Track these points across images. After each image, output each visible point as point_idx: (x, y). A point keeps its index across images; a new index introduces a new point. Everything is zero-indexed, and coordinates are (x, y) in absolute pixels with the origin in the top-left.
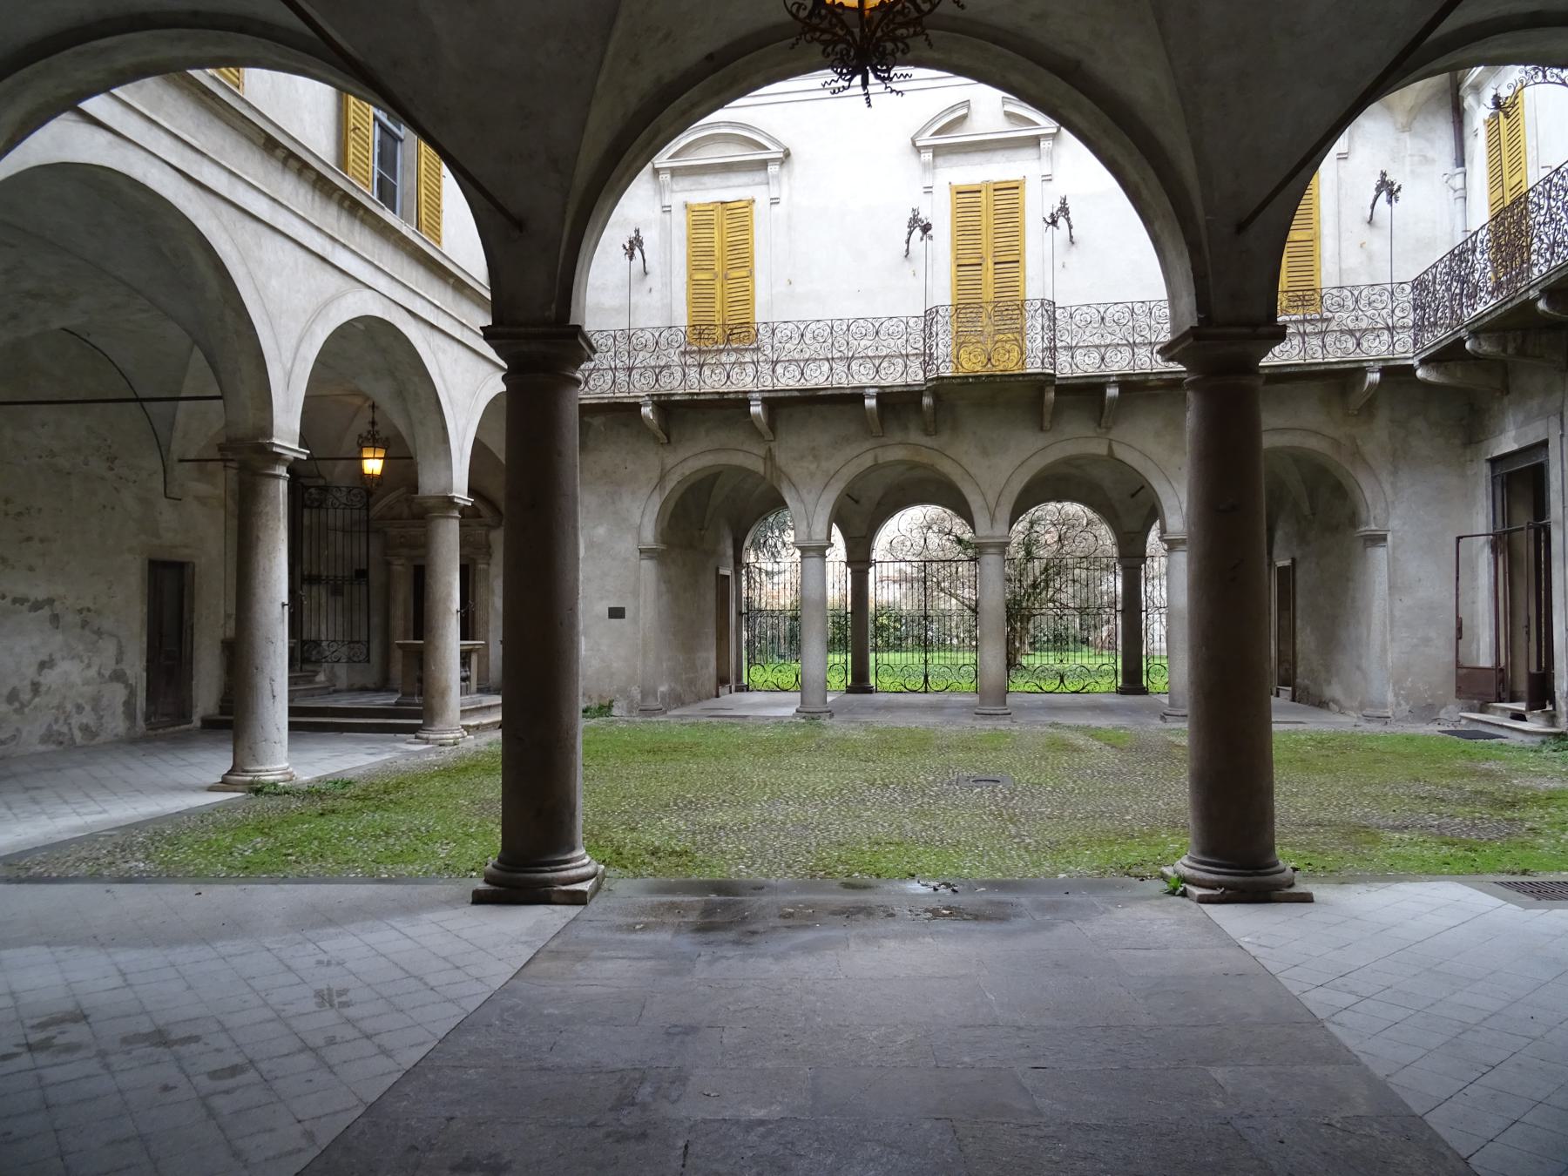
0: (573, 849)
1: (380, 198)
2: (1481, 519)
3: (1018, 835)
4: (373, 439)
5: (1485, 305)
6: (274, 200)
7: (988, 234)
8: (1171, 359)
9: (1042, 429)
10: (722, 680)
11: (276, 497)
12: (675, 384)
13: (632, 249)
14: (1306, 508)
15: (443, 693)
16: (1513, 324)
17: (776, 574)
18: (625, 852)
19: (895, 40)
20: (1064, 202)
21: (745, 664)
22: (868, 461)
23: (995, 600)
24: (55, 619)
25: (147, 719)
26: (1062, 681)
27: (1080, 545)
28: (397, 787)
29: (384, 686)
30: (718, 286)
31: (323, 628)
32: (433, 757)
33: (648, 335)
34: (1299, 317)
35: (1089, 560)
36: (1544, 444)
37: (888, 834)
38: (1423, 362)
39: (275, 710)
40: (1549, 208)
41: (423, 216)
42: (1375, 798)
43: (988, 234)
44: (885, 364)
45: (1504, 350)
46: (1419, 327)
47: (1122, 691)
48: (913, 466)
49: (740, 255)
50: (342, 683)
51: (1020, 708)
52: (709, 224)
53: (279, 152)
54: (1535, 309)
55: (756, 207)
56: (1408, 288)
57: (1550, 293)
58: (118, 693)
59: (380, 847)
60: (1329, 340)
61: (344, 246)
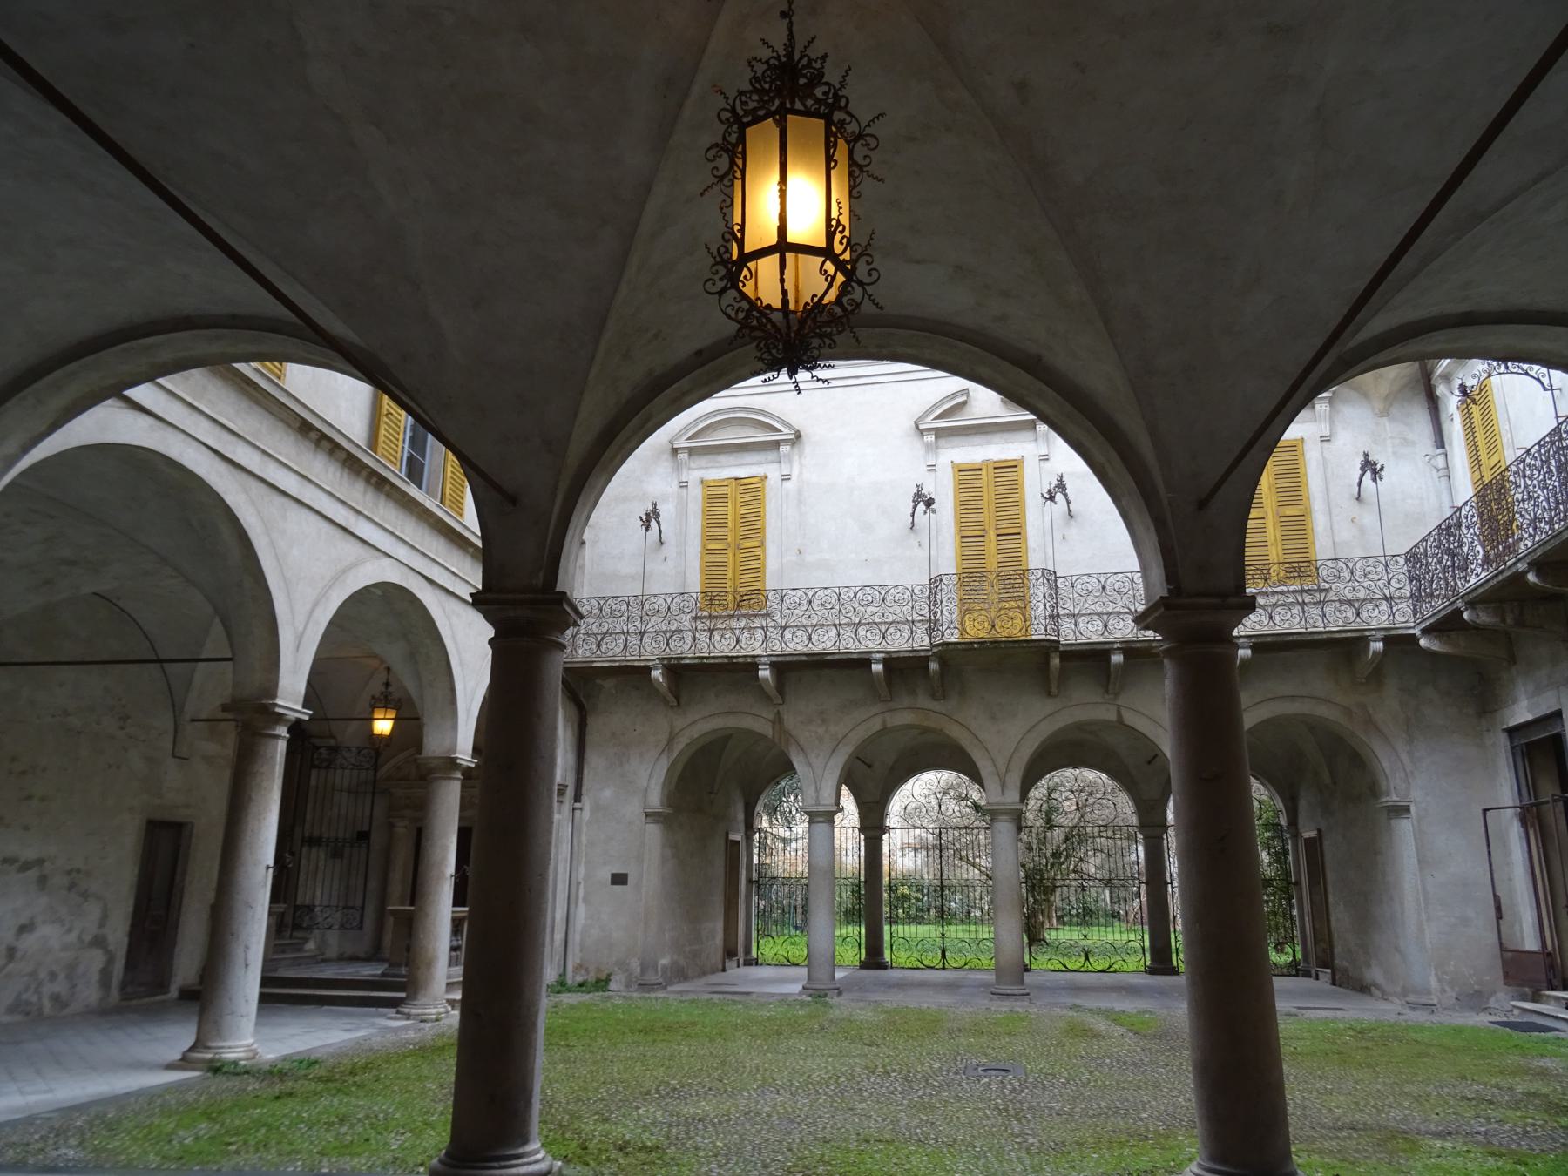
0: (526, 1141)
1: (409, 476)
2: (1505, 790)
3: (1022, 1134)
4: (385, 700)
5: (1477, 576)
6: (303, 477)
7: (990, 504)
8: (1146, 628)
9: (1049, 694)
10: (730, 953)
11: (273, 758)
12: (684, 648)
13: (648, 521)
14: (1326, 777)
15: (430, 965)
16: (1505, 594)
17: (784, 843)
18: (591, 1146)
19: (821, 336)
20: (1060, 479)
21: (754, 935)
22: (876, 725)
23: (1010, 875)
24: (42, 881)
25: (123, 987)
26: (1087, 958)
27: (1101, 813)
28: (366, 1067)
29: (373, 956)
30: (731, 555)
31: (318, 893)
32: (411, 1034)
33: (661, 601)
34: (1298, 588)
35: (1111, 828)
36: (1558, 715)
37: (879, 1131)
38: (1425, 631)
39: (247, 982)
40: (1526, 486)
41: (448, 491)
42: (1417, 1099)
43: (990, 504)
44: (891, 630)
45: (1503, 621)
46: (1416, 598)
47: (1151, 971)
48: (925, 730)
49: (753, 526)
50: (332, 952)
51: (1041, 988)
52: (723, 498)
53: (313, 435)
54: (1526, 582)
55: (767, 483)
56: (1401, 561)
57: (1538, 565)
58: (96, 959)
59: (330, 1137)
60: (1328, 609)
61: (368, 518)
